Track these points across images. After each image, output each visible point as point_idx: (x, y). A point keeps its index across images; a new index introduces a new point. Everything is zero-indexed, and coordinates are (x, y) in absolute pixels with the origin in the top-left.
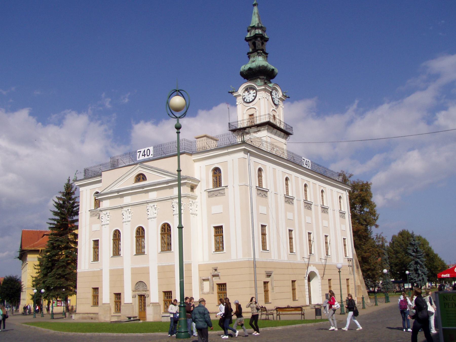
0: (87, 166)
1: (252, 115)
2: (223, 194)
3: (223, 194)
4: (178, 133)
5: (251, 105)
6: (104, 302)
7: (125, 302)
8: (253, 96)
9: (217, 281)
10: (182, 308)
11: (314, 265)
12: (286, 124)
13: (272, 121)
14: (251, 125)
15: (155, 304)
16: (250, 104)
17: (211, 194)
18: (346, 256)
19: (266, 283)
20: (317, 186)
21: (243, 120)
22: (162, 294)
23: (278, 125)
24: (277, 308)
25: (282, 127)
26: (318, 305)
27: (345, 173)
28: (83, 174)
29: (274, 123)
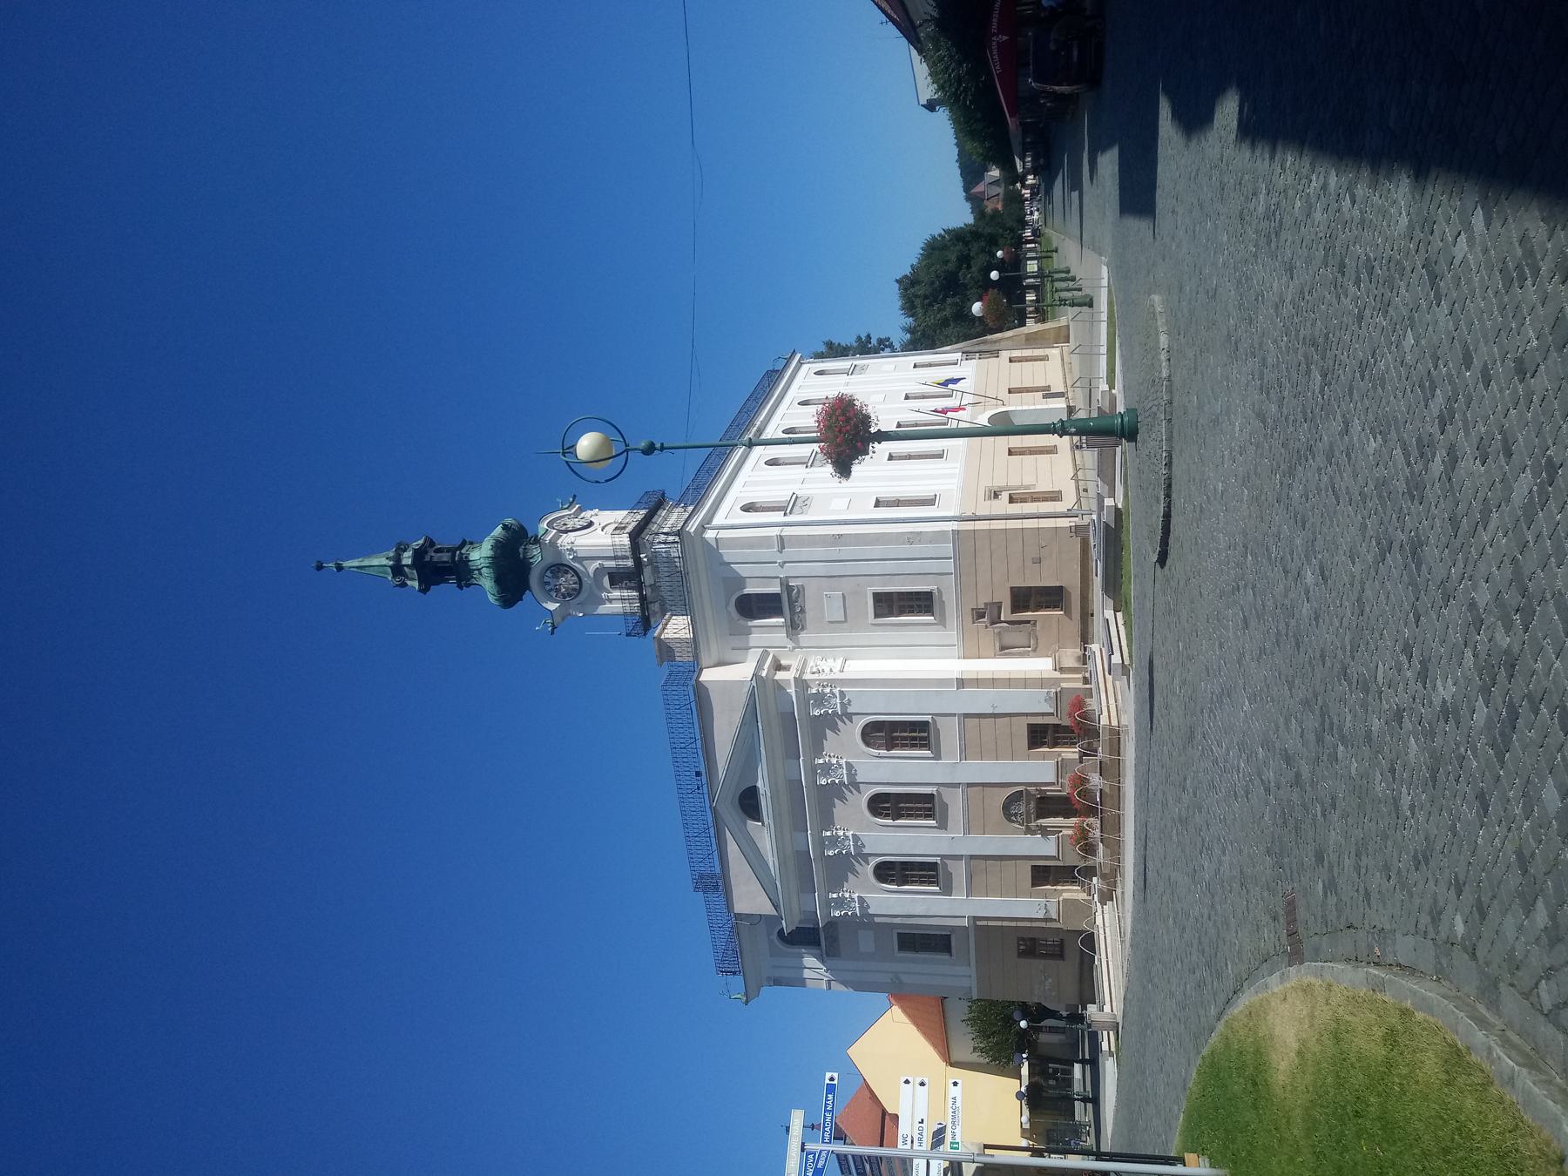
2: (801, 590)
3: (801, 590)
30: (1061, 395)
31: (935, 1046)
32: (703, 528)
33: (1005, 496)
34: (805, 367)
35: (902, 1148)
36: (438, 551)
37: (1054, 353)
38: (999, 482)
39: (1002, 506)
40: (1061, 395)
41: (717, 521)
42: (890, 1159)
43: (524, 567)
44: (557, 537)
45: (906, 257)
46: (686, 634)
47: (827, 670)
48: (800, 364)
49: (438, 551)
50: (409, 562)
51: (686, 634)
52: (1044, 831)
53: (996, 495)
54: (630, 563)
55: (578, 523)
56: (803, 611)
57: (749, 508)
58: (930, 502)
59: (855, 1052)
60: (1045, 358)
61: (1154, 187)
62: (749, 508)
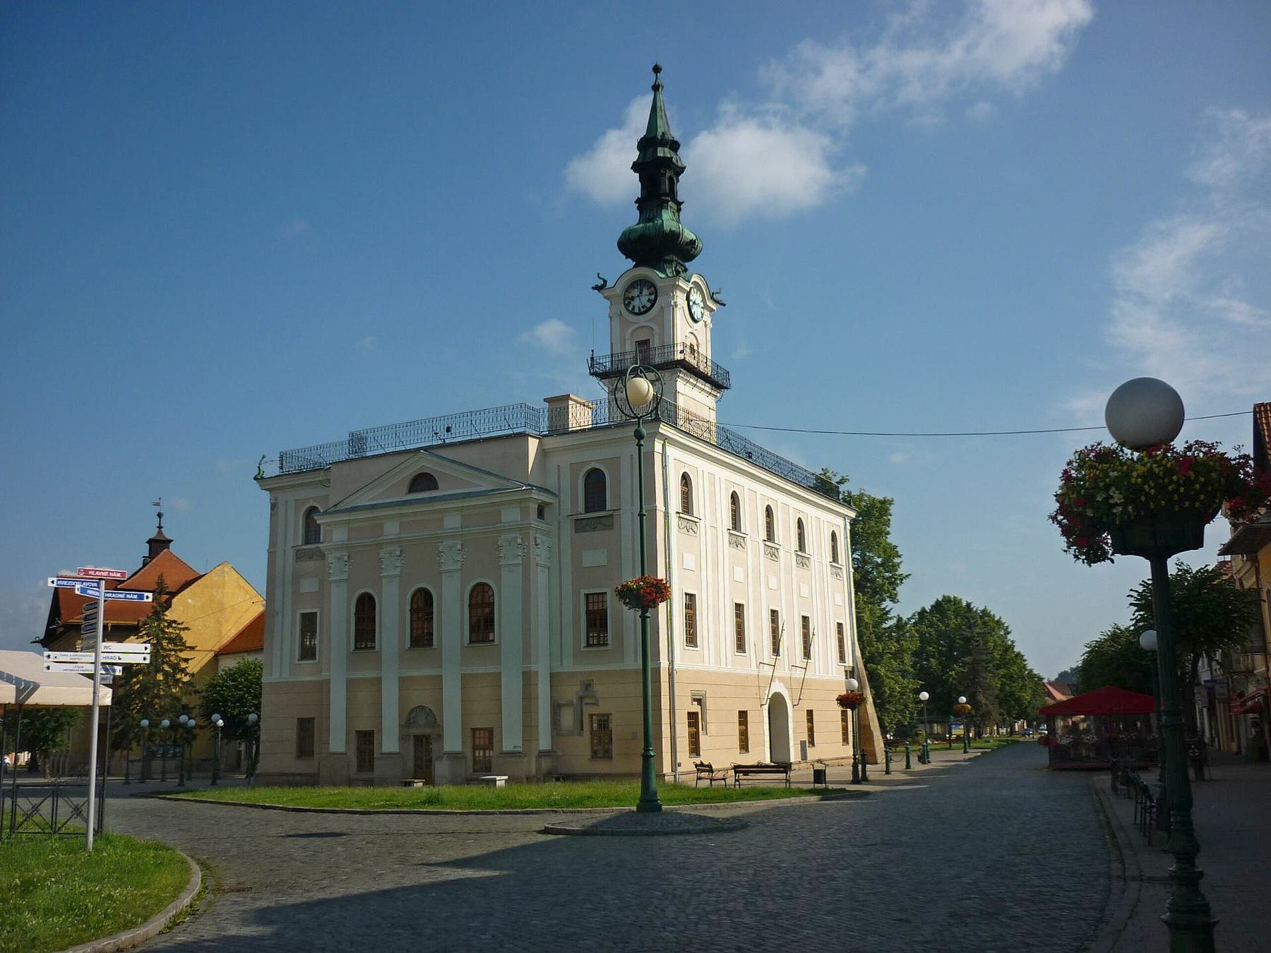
0: (284, 449)
1: (646, 342)
2: (611, 527)
3: (611, 527)
4: (640, 446)
5: (642, 320)
6: (331, 750)
7: (385, 750)
8: (649, 300)
9: (588, 710)
10: (193, 775)
11: (781, 679)
12: (716, 366)
13: (690, 359)
14: (665, 375)
15: (453, 756)
16: (641, 317)
17: (580, 526)
18: (842, 659)
19: (692, 716)
20: (791, 510)
21: (623, 354)
22: (353, 737)
23: (702, 368)
24: (735, 767)
25: (709, 371)
26: (820, 761)
27: (829, 474)
28: (278, 464)
29: (694, 362)
30: (804, 756)
31: (233, 641)
32: (665, 439)
33: (696, 708)
34: (840, 521)
35: (103, 646)
36: (671, 180)
37: (849, 751)
38: (709, 704)
39: (685, 706)
40: (804, 756)
41: (670, 450)
42: (95, 637)
43: (657, 263)
44: (683, 290)
45: (1081, 566)
46: (573, 425)
47: (538, 552)
48: (844, 517)
49: (671, 180)
50: (660, 154)
51: (573, 425)
52: (403, 738)
53: (699, 701)
54: (658, 360)
55: (697, 311)
56: (594, 529)
57: (686, 479)
58: (691, 639)
59: (13, 701)
60: (845, 740)
61: (1191, 806)
62: (686, 479)
